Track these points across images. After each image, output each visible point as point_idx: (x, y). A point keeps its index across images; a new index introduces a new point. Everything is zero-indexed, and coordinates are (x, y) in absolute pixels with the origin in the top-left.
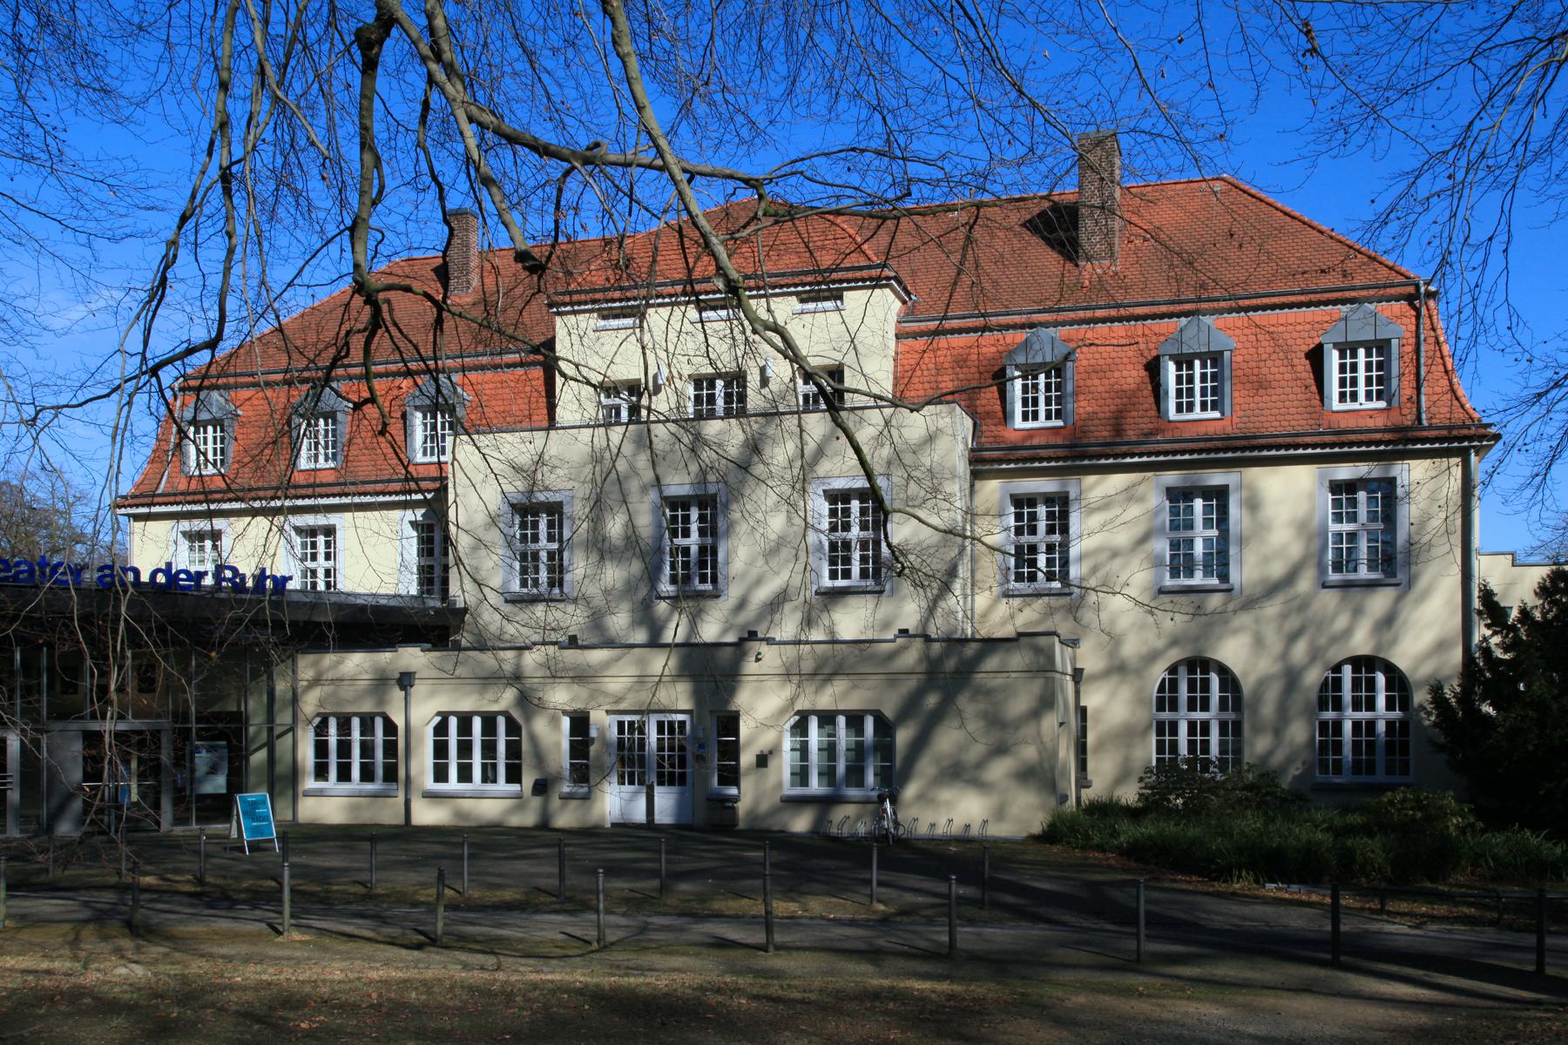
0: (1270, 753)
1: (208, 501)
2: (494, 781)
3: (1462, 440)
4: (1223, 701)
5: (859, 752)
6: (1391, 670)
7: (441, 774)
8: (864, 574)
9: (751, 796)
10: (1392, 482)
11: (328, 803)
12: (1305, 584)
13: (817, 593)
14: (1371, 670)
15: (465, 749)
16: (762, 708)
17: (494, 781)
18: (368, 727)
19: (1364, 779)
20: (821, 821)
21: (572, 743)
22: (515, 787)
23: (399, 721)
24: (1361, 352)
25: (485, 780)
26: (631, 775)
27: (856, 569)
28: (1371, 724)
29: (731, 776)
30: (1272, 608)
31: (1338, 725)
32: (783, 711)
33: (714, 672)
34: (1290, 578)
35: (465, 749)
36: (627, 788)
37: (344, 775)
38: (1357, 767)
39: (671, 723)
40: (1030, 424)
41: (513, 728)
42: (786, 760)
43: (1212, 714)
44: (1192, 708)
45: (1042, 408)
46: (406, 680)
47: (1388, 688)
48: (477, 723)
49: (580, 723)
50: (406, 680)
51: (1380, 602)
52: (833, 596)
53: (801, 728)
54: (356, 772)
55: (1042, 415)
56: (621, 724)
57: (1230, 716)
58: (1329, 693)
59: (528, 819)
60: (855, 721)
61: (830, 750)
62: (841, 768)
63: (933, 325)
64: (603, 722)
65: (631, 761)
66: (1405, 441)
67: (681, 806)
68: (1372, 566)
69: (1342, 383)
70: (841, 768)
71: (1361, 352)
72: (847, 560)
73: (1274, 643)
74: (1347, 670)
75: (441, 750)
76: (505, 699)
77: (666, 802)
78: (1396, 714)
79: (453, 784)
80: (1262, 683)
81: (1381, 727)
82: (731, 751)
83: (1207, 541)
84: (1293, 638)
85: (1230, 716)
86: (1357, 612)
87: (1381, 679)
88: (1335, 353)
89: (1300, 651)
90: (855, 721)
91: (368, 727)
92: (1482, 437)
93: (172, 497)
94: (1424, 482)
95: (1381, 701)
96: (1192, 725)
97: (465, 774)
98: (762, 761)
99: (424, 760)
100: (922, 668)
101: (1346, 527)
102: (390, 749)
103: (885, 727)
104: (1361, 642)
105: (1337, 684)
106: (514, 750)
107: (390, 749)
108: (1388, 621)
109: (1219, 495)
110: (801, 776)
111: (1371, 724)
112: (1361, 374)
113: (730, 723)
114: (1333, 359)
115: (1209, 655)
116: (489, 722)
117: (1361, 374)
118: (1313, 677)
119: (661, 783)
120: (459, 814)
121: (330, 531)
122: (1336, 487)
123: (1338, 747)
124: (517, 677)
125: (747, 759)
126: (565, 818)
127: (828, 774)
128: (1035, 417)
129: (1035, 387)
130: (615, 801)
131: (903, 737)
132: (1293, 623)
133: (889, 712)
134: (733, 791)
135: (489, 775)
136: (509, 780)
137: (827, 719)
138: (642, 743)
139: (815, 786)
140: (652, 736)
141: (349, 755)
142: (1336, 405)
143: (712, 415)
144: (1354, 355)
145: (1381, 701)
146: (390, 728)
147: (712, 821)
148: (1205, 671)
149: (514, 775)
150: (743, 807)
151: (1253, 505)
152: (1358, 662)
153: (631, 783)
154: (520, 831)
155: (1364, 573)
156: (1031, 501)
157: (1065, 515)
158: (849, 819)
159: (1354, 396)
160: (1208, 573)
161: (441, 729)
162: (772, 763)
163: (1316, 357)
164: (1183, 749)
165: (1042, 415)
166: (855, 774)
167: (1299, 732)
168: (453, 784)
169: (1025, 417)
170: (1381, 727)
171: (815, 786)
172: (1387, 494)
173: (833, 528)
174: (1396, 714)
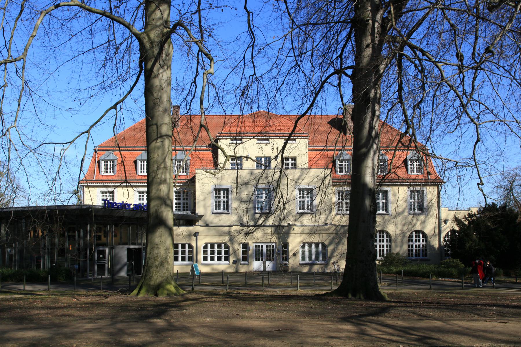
0: (400, 251)
1: (87, 183)
2: (207, 260)
3: (438, 183)
4: (423, 240)
5: (317, 253)
6: (423, 233)
7: (205, 259)
8: (224, 209)
9: (293, 262)
10: (423, 191)
11: (178, 267)
12: (406, 214)
13: (297, 213)
14: (419, 233)
15: (212, 253)
16: (294, 242)
17: (207, 260)
18: (183, 246)
19: (425, 257)
20: (310, 269)
21: (243, 251)
22: (227, 262)
23: (194, 245)
24: (109, 162)
25: (182, 261)
26: (259, 258)
27: (222, 207)
28: (419, 245)
29: (287, 259)
30: (399, 219)
31: (412, 246)
32: (300, 242)
33: (282, 231)
34: (403, 212)
35: (212, 253)
36: (258, 262)
37: (183, 259)
38: (416, 255)
39: (259, 246)
40: (341, 174)
41: (227, 247)
42: (300, 255)
43: (385, 243)
44: (380, 241)
45: (344, 170)
46: (196, 235)
47: (387, 237)
48: (216, 246)
49: (245, 246)
50: (196, 235)
51: (422, 217)
52: (302, 214)
53: (303, 247)
54: (180, 259)
55: (109, 172)
56: (256, 246)
57: (389, 243)
58: (410, 239)
59: (231, 270)
60: (317, 245)
61: (310, 252)
62: (314, 257)
63: (322, 148)
64: (252, 246)
65: (259, 255)
66: (427, 183)
67: (274, 266)
68: (419, 210)
69: (141, 169)
70: (314, 257)
71: (109, 162)
72: (219, 205)
73: (400, 227)
74: (414, 233)
75: (205, 252)
76: (225, 239)
77: (269, 266)
78: (424, 243)
79: (209, 261)
80: (397, 235)
81: (421, 246)
82: (287, 252)
83: (383, 203)
84: (404, 225)
85: (389, 243)
86: (417, 220)
87: (421, 235)
88: (140, 162)
89: (405, 228)
90: (317, 245)
91: (183, 246)
92: (441, 182)
93: (97, 181)
94: (430, 192)
95: (421, 240)
96: (380, 246)
97: (212, 259)
98: (294, 255)
99: (201, 256)
100: (335, 232)
101: (413, 201)
102: (191, 252)
103: (324, 246)
104: (418, 227)
105: (412, 236)
106: (227, 252)
107: (191, 252)
108: (424, 222)
109: (386, 192)
110: (303, 258)
111: (419, 245)
112: (109, 167)
113: (286, 245)
114: (102, 163)
115: (385, 229)
116: (219, 245)
117: (109, 167)
118: (408, 234)
119: (267, 260)
120: (213, 269)
121: (113, 192)
122: (412, 191)
123: (412, 250)
124: (229, 233)
125: (291, 254)
126: (243, 269)
127: (310, 258)
128: (342, 172)
129: (342, 165)
130: (256, 265)
131: (330, 249)
132: (404, 222)
133: (326, 243)
134: (286, 262)
135: (219, 259)
136: (225, 260)
137: (310, 245)
138: (262, 250)
139: (307, 260)
140: (265, 249)
141: (214, 254)
142: (140, 174)
143: (288, 168)
144: (107, 163)
145: (421, 240)
146: (190, 247)
147: (282, 270)
148: (383, 233)
149: (227, 259)
150: (290, 266)
151: (394, 195)
152: (417, 232)
153: (259, 260)
154: (230, 273)
155: (222, 210)
156: (106, 192)
157: (228, 194)
158: (316, 268)
159: (107, 172)
160: (383, 210)
161: (205, 247)
162: (297, 255)
163: (135, 162)
164: (414, 251)
165: (109, 172)
166: (317, 258)
167: (405, 247)
168: (209, 261)
169: (340, 172)
170: (421, 246)
171: (307, 260)
172: (421, 194)
173: (300, 197)
174: (424, 243)
